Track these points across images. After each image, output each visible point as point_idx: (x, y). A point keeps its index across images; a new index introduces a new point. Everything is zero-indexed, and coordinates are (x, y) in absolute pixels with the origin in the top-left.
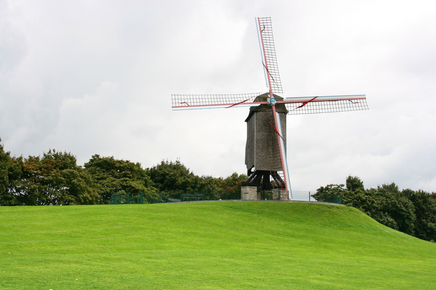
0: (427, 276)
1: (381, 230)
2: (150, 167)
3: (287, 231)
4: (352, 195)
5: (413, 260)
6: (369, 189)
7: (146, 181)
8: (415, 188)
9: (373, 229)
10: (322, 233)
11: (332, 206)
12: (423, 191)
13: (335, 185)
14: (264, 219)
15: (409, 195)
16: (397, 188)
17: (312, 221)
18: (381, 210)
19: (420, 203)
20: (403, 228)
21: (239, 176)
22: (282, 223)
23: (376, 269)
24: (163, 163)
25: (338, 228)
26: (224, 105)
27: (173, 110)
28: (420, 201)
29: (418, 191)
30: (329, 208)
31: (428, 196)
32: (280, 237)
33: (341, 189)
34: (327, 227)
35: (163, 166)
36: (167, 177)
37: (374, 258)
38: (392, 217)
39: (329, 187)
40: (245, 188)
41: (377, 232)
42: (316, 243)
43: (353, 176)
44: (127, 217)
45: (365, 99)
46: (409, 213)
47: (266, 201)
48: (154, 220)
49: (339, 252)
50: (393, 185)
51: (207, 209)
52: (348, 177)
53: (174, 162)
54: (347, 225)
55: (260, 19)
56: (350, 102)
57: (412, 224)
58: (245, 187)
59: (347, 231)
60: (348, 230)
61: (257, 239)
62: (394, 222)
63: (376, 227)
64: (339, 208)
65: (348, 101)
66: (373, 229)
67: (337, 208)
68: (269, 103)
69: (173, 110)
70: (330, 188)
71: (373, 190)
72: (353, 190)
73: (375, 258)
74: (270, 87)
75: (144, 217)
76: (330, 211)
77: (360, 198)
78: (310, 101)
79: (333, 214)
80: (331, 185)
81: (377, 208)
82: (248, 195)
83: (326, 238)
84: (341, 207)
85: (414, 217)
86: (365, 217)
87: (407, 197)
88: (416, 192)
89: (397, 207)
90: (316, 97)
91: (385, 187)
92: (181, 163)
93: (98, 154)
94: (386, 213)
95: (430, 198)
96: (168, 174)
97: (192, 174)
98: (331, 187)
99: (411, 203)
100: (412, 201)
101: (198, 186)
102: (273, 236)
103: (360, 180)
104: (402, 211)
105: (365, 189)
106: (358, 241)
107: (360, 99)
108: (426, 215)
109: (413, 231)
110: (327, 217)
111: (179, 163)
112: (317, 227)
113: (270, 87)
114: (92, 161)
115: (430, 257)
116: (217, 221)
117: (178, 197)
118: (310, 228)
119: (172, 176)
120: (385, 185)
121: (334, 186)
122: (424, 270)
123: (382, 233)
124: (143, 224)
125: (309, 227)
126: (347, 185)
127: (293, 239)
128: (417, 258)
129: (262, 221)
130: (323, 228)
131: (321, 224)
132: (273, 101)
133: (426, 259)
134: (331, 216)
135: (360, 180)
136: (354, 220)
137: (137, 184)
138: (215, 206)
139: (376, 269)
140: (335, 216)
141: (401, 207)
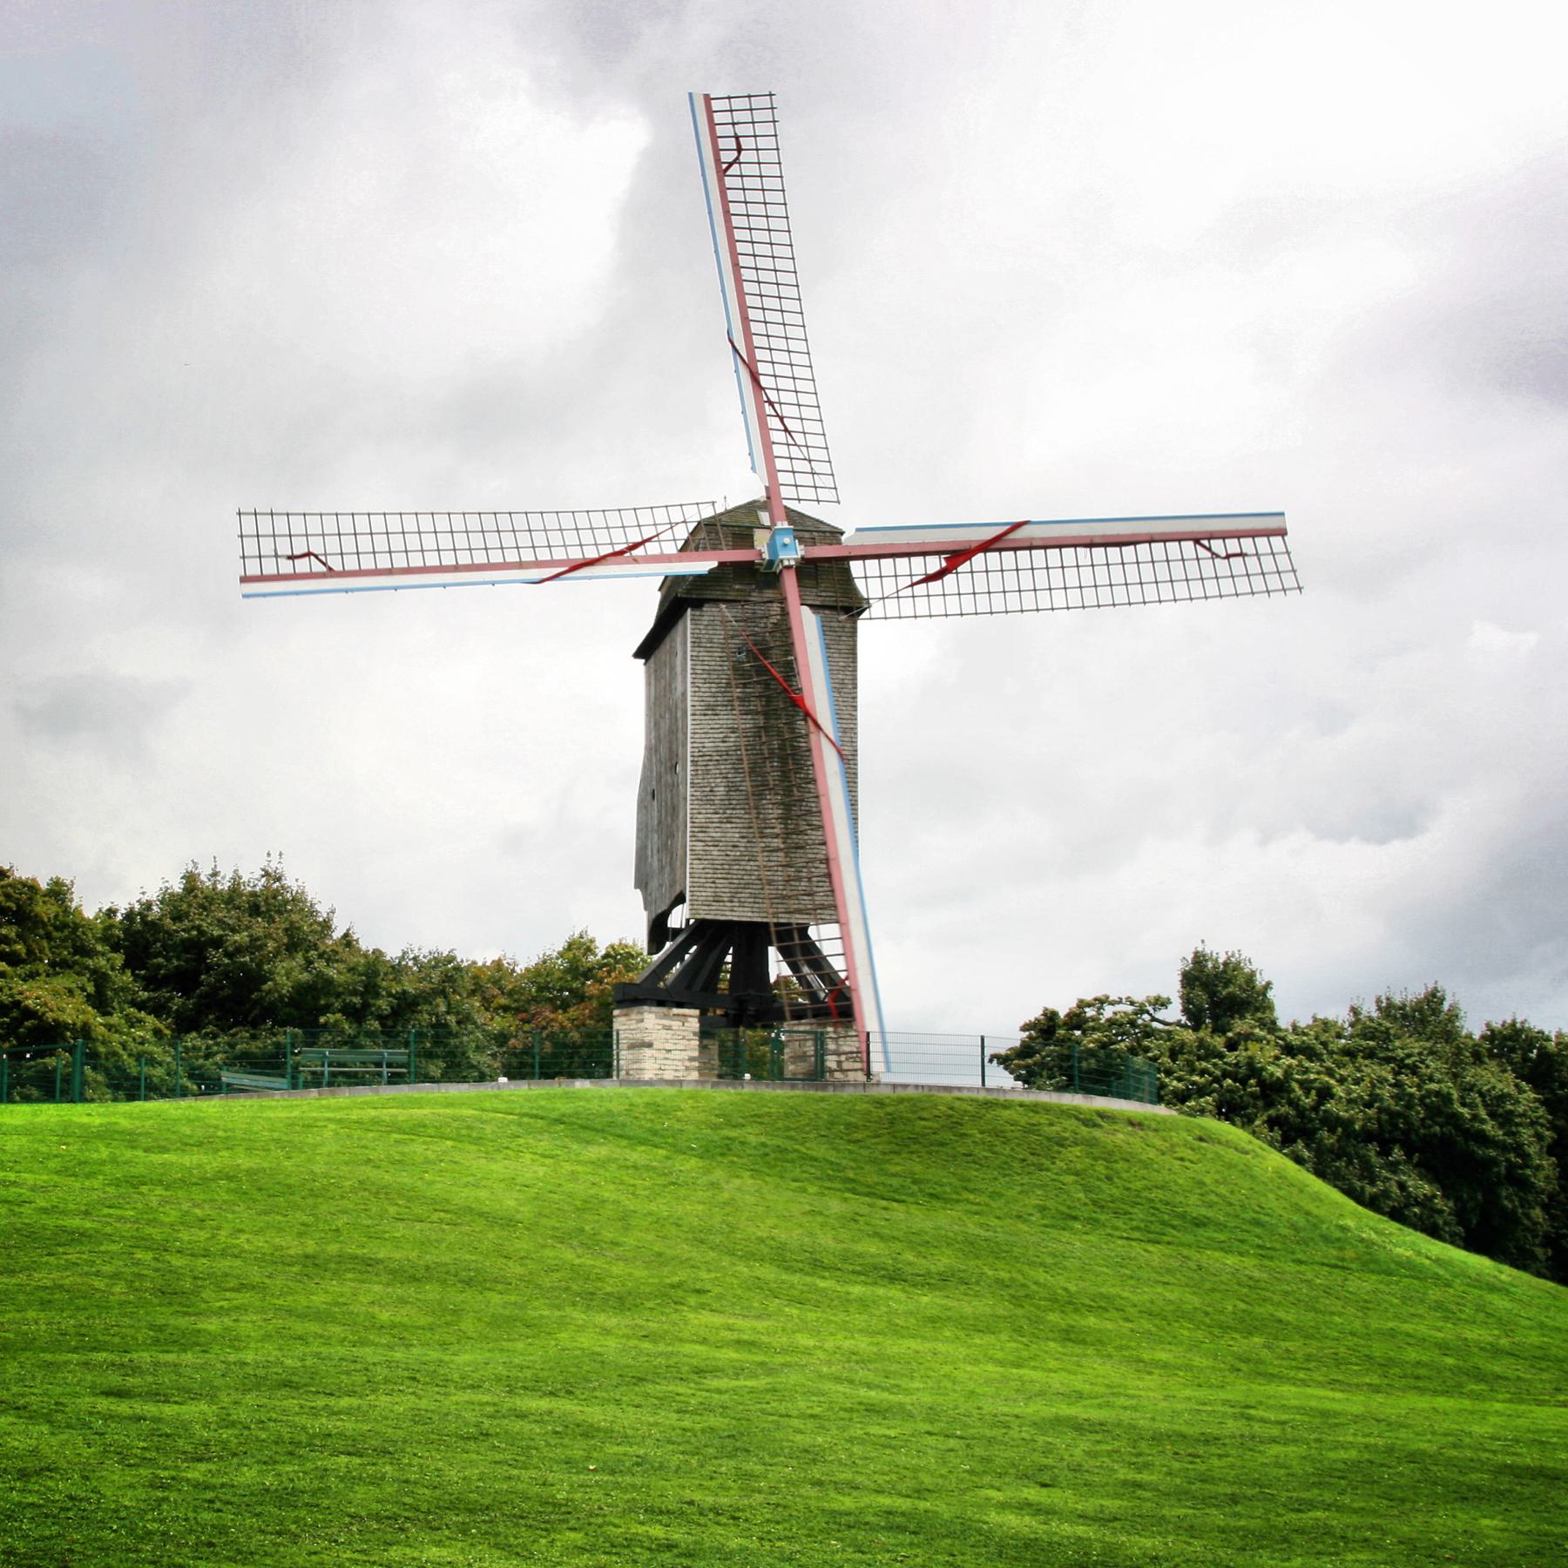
1: (1369, 1244)
2: (124, 903)
3: (859, 1248)
5: (1541, 1403)
7: (100, 978)
10: (1049, 1260)
11: (1102, 1115)
13: (1120, 1002)
14: (737, 1182)
15: (1516, 1057)
16: (1453, 1016)
17: (995, 1195)
18: (1367, 1136)
21: (601, 952)
22: (835, 1206)
23: (1342, 1454)
24: (190, 879)
25: (1136, 1235)
26: (521, 565)
27: (245, 596)
32: (822, 1284)
33: (1154, 1019)
34: (1078, 1226)
37: (1330, 1394)
38: (1428, 1170)
39: (1090, 1012)
42: (1019, 1312)
45: (1282, 533)
46: (1519, 1149)
47: (747, 1091)
48: (144, 1189)
49: (1140, 1360)
50: (1433, 999)
51: (431, 1131)
52: (1190, 957)
53: (252, 877)
54: (1183, 1216)
55: (715, 105)
56: (1203, 553)
57: (1537, 1213)
58: (634, 1013)
59: (1185, 1252)
61: (698, 1292)
62: (1439, 1202)
63: (1344, 1229)
65: (1188, 546)
66: (1326, 1239)
67: (1131, 1123)
68: (766, 556)
69: (245, 596)
70: (1093, 1019)
72: (1219, 1029)
74: (772, 472)
75: (88, 1176)
76: (1092, 1143)
77: (1253, 1070)
78: (986, 547)
79: (1108, 1156)
80: (1101, 1002)
82: (647, 1052)
83: (1073, 1288)
84: (1154, 1118)
87: (1510, 1062)
89: (1455, 1118)
90: (1017, 526)
91: (1388, 1009)
92: (289, 881)
94: (1397, 1153)
96: (217, 943)
97: (348, 941)
99: (1527, 1099)
100: (1537, 1088)
102: (784, 1277)
103: (1253, 974)
104: (1483, 1139)
105: (1284, 1023)
106: (1242, 1306)
107: (1239, 538)
109: (1539, 1251)
110: (1077, 1174)
111: (279, 879)
113: (772, 472)
118: (983, 1233)
119: (239, 950)
120: (1388, 999)
121: (1112, 1003)
125: (981, 1225)
126: (1187, 1001)
127: (895, 1292)
129: (726, 1195)
130: (1054, 1233)
131: (1042, 1209)
132: (785, 545)
134: (1100, 1167)
135: (1253, 974)
136: (1222, 1190)
138: (471, 1112)
140: (1120, 1166)
141: (1475, 1117)
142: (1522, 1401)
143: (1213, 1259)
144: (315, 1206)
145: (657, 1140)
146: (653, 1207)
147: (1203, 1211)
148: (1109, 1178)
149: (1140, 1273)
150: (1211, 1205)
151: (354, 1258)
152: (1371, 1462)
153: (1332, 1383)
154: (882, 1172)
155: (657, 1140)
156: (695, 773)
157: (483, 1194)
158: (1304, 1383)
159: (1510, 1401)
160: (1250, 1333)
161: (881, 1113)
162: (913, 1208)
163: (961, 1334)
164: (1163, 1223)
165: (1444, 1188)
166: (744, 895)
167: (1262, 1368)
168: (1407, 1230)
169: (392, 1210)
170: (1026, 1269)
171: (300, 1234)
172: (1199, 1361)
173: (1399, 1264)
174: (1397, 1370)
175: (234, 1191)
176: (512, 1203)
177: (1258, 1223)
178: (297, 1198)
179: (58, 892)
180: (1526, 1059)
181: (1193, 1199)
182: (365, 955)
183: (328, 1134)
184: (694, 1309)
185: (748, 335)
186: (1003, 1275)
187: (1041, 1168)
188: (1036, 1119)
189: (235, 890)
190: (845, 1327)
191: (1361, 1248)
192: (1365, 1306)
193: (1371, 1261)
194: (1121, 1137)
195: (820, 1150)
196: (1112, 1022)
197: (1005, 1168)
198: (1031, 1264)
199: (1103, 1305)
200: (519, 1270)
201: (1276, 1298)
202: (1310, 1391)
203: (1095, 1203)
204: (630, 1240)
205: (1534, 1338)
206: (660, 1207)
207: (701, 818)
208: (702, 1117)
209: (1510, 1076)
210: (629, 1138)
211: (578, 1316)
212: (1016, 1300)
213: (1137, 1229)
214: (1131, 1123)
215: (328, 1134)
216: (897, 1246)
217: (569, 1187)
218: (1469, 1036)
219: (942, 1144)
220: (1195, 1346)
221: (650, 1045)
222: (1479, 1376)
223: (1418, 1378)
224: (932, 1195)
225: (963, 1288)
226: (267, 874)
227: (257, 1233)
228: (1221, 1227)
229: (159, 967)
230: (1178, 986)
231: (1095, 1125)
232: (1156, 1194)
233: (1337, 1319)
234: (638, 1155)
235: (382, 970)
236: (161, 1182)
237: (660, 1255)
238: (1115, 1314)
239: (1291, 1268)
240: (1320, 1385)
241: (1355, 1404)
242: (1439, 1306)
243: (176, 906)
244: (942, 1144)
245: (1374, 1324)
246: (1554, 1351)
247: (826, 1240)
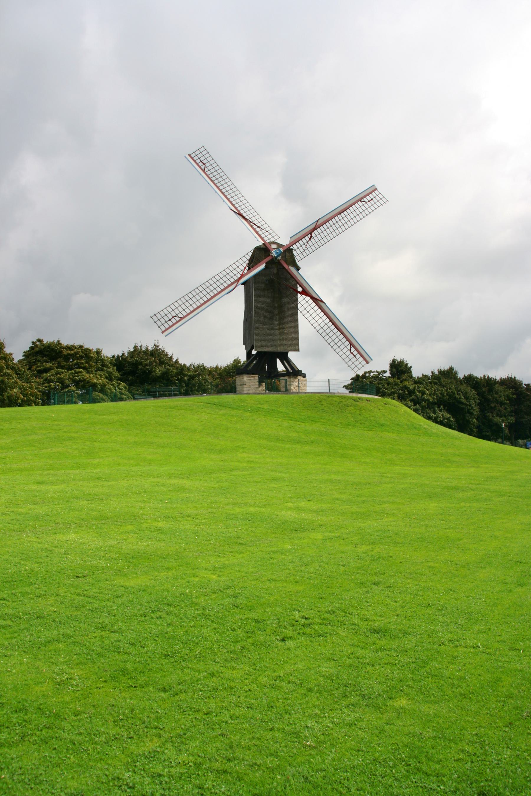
0: (472, 492)
2: (118, 353)
4: (396, 384)
5: (463, 467)
6: (420, 376)
7: (110, 373)
8: (479, 374)
9: (415, 428)
10: (341, 436)
11: (360, 398)
12: (488, 377)
13: (374, 372)
15: (471, 383)
16: (456, 373)
19: (484, 392)
21: (242, 362)
22: (286, 424)
23: (403, 486)
24: (135, 347)
25: (366, 429)
26: (222, 291)
27: (166, 336)
29: (483, 376)
30: (355, 400)
31: (495, 382)
32: (278, 445)
34: (351, 427)
35: (136, 352)
36: (140, 367)
37: (409, 468)
38: (449, 411)
39: (367, 375)
40: (241, 377)
43: (399, 358)
44: (56, 423)
45: (376, 189)
46: (470, 405)
48: (95, 425)
50: (451, 369)
52: (392, 360)
53: (151, 347)
54: (378, 424)
57: (475, 420)
59: (378, 433)
61: (243, 448)
62: (452, 419)
63: (420, 425)
66: (415, 428)
70: (368, 376)
72: (399, 378)
73: (411, 468)
76: (356, 406)
77: (406, 387)
80: (370, 372)
81: (428, 400)
82: (245, 386)
83: (347, 443)
84: (373, 398)
85: (476, 410)
86: (405, 412)
87: (469, 384)
89: (455, 398)
91: (441, 372)
92: (161, 347)
93: (41, 338)
94: (442, 407)
95: (497, 385)
96: (141, 363)
97: (177, 361)
98: (370, 374)
99: (472, 393)
103: (407, 364)
104: (462, 403)
105: (414, 376)
108: (491, 407)
109: (475, 430)
111: (158, 347)
112: (336, 428)
114: (32, 348)
115: (487, 463)
117: (151, 394)
118: (325, 430)
119: (146, 365)
121: (373, 372)
122: (472, 482)
123: (426, 433)
126: (391, 370)
128: (469, 466)
131: (341, 423)
134: (358, 412)
135: (407, 364)
136: (390, 417)
137: (99, 380)
139: (403, 486)
140: (363, 411)
141: (460, 398)
145: (240, 408)
147: (384, 422)
148: (360, 415)
150: (386, 420)
152: (410, 488)
156: (255, 313)
162: (307, 424)
164: (373, 426)
169: (163, 429)
177: (398, 425)
179: (98, 352)
180: (473, 383)
185: (233, 205)
189: (147, 349)
193: (426, 433)
194: (364, 404)
196: (372, 377)
218: (460, 378)
221: (245, 385)
226: (155, 345)
229: (127, 370)
230: (389, 368)
232: (372, 418)
233: (415, 448)
234: (234, 412)
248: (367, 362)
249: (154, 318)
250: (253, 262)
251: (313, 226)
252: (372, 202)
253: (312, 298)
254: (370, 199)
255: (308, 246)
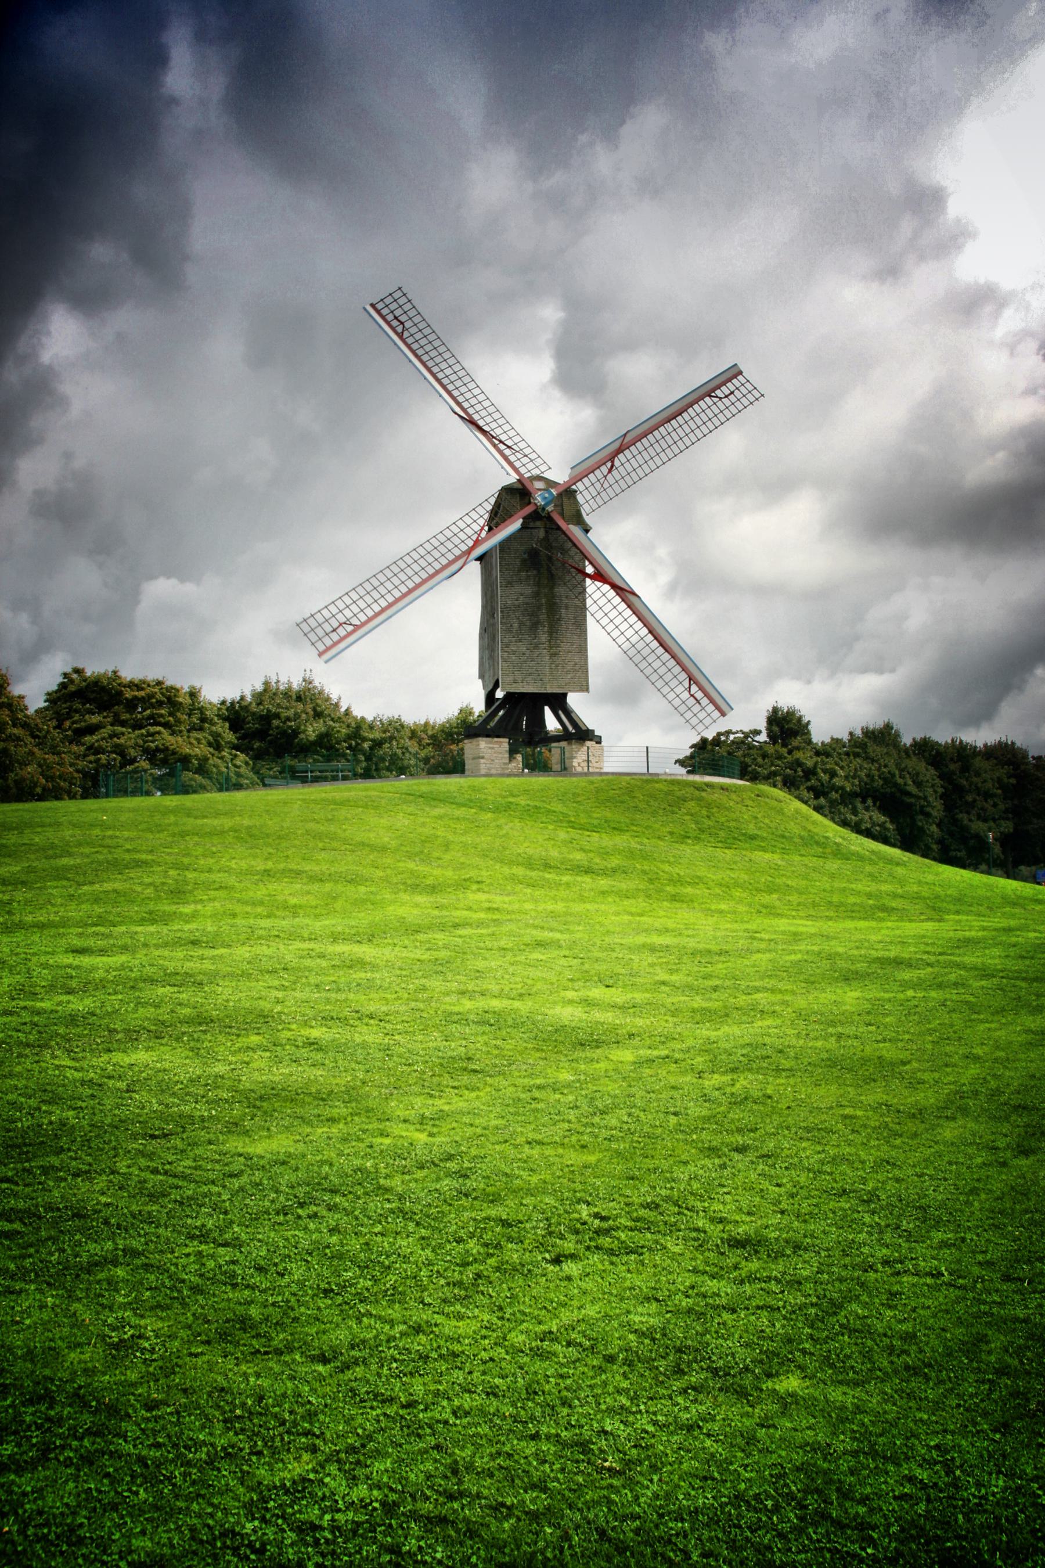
1: (837, 844)
3: (571, 857)
4: (780, 757)
5: (910, 921)
6: (827, 740)
7: (217, 736)
10: (672, 860)
12: (961, 741)
14: (511, 824)
15: (927, 754)
16: (897, 735)
17: (647, 827)
18: (854, 795)
19: (953, 773)
20: (910, 842)
21: (477, 714)
22: (562, 835)
23: (793, 957)
24: (266, 683)
25: (720, 845)
27: (326, 662)
28: (952, 767)
29: (949, 741)
30: (698, 789)
32: (547, 876)
34: (690, 841)
35: (267, 693)
36: (275, 723)
38: (883, 809)
41: (828, 850)
42: (651, 886)
46: (925, 798)
47: (540, 781)
48: (187, 838)
49: (709, 909)
50: (888, 727)
51: (352, 804)
52: (771, 709)
53: (296, 684)
54: (744, 835)
57: (934, 828)
58: (475, 741)
59: (744, 853)
60: (746, 849)
61: (478, 882)
63: (827, 838)
64: (727, 790)
66: (817, 843)
67: (722, 789)
70: (725, 741)
71: (836, 741)
72: (784, 745)
75: (159, 832)
76: (700, 799)
77: (799, 763)
79: (708, 806)
80: (728, 733)
81: (843, 788)
82: (482, 761)
83: (682, 874)
84: (735, 785)
85: (937, 808)
87: (924, 757)
88: (946, 743)
89: (896, 785)
91: (868, 733)
92: (316, 683)
93: (81, 667)
94: (870, 802)
96: (277, 716)
97: (347, 713)
98: (727, 737)
99: (929, 774)
100: (936, 768)
101: (366, 745)
102: (528, 873)
104: (909, 794)
105: (814, 741)
106: (770, 879)
108: (966, 802)
109: (934, 847)
110: (692, 815)
111: (310, 683)
112: (661, 843)
114: (63, 686)
116: (372, 835)
118: (639, 847)
119: (288, 719)
121: (734, 733)
122: (929, 949)
123: (839, 853)
124: (152, 851)
125: (638, 843)
127: (587, 879)
128: (922, 917)
129: (504, 832)
130: (677, 846)
131: (671, 833)
133: (947, 917)
134: (704, 812)
136: (767, 821)
138: (376, 793)
139: (793, 957)
140: (715, 810)
141: (905, 784)
142: (902, 921)
143: (759, 856)
144: (279, 844)
146: (463, 839)
147: (756, 832)
148: (708, 817)
149: (719, 865)
151: (291, 870)
153: (808, 917)
154: (590, 817)
155: (472, 804)
157: (372, 835)
158: (794, 917)
159: (897, 921)
160: (771, 893)
161: (592, 787)
162: (604, 835)
163: (617, 900)
165: (890, 816)
166: (529, 679)
167: (773, 911)
168: (860, 837)
169: (320, 845)
170: (659, 864)
171: (266, 859)
172: (741, 908)
173: (853, 854)
174: (843, 908)
175: (237, 837)
176: (386, 839)
177: (783, 837)
178: (270, 840)
181: (751, 826)
182: (355, 718)
183: (296, 806)
184: (473, 892)
185: (459, 404)
186: (646, 868)
187: (673, 813)
188: (672, 788)
190: (554, 899)
191: (835, 847)
192: (832, 876)
195: (558, 807)
196: (733, 742)
197: (654, 814)
198: (663, 862)
199: (697, 881)
200: (381, 874)
201: (788, 874)
202: (795, 921)
203: (700, 829)
204: (447, 857)
205: (915, 888)
206: (468, 839)
207: (506, 640)
208: (498, 792)
209: (923, 764)
210: (456, 804)
211: (405, 897)
212: (651, 881)
213: (721, 842)
214: (722, 789)
215: (296, 806)
216: (591, 855)
217: (420, 830)
218: (905, 745)
219: (622, 802)
220: (740, 901)
221: (483, 758)
222: (884, 909)
223: (853, 911)
224: (614, 828)
225: (624, 875)
226: (304, 680)
227: (241, 859)
228: (763, 839)
229: (250, 728)
231: (704, 790)
232: (732, 824)
233: (818, 883)
235: (365, 726)
236: (197, 834)
237: (463, 863)
238: (701, 885)
239: (797, 858)
240: (801, 918)
241: (808, 927)
242: (870, 875)
243: (259, 697)
244: (622, 802)
245: (836, 885)
246: (923, 894)
247: (554, 853)
248: (723, 714)
249: (304, 626)
250: (497, 517)
251: (617, 445)
252: (732, 397)
253: (614, 586)
254: (727, 392)
255: (606, 485)
